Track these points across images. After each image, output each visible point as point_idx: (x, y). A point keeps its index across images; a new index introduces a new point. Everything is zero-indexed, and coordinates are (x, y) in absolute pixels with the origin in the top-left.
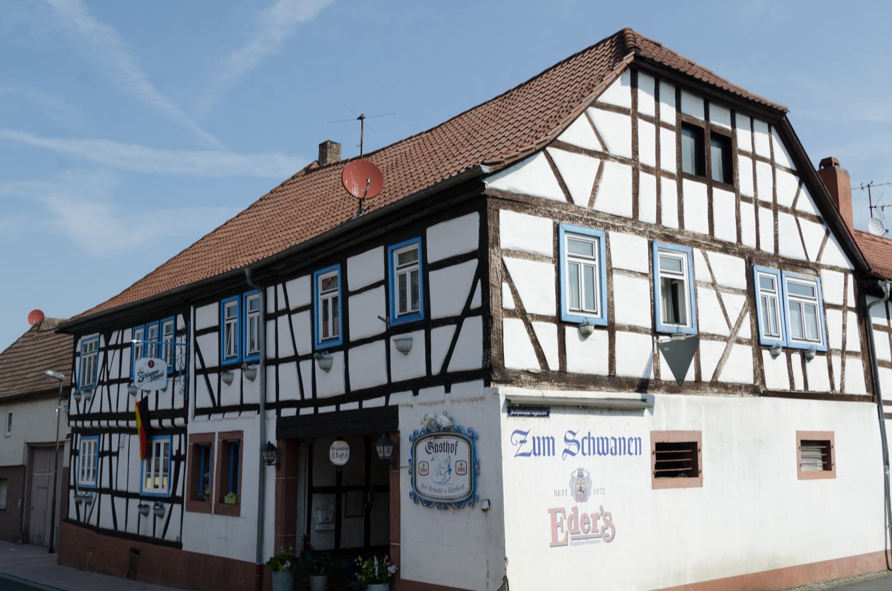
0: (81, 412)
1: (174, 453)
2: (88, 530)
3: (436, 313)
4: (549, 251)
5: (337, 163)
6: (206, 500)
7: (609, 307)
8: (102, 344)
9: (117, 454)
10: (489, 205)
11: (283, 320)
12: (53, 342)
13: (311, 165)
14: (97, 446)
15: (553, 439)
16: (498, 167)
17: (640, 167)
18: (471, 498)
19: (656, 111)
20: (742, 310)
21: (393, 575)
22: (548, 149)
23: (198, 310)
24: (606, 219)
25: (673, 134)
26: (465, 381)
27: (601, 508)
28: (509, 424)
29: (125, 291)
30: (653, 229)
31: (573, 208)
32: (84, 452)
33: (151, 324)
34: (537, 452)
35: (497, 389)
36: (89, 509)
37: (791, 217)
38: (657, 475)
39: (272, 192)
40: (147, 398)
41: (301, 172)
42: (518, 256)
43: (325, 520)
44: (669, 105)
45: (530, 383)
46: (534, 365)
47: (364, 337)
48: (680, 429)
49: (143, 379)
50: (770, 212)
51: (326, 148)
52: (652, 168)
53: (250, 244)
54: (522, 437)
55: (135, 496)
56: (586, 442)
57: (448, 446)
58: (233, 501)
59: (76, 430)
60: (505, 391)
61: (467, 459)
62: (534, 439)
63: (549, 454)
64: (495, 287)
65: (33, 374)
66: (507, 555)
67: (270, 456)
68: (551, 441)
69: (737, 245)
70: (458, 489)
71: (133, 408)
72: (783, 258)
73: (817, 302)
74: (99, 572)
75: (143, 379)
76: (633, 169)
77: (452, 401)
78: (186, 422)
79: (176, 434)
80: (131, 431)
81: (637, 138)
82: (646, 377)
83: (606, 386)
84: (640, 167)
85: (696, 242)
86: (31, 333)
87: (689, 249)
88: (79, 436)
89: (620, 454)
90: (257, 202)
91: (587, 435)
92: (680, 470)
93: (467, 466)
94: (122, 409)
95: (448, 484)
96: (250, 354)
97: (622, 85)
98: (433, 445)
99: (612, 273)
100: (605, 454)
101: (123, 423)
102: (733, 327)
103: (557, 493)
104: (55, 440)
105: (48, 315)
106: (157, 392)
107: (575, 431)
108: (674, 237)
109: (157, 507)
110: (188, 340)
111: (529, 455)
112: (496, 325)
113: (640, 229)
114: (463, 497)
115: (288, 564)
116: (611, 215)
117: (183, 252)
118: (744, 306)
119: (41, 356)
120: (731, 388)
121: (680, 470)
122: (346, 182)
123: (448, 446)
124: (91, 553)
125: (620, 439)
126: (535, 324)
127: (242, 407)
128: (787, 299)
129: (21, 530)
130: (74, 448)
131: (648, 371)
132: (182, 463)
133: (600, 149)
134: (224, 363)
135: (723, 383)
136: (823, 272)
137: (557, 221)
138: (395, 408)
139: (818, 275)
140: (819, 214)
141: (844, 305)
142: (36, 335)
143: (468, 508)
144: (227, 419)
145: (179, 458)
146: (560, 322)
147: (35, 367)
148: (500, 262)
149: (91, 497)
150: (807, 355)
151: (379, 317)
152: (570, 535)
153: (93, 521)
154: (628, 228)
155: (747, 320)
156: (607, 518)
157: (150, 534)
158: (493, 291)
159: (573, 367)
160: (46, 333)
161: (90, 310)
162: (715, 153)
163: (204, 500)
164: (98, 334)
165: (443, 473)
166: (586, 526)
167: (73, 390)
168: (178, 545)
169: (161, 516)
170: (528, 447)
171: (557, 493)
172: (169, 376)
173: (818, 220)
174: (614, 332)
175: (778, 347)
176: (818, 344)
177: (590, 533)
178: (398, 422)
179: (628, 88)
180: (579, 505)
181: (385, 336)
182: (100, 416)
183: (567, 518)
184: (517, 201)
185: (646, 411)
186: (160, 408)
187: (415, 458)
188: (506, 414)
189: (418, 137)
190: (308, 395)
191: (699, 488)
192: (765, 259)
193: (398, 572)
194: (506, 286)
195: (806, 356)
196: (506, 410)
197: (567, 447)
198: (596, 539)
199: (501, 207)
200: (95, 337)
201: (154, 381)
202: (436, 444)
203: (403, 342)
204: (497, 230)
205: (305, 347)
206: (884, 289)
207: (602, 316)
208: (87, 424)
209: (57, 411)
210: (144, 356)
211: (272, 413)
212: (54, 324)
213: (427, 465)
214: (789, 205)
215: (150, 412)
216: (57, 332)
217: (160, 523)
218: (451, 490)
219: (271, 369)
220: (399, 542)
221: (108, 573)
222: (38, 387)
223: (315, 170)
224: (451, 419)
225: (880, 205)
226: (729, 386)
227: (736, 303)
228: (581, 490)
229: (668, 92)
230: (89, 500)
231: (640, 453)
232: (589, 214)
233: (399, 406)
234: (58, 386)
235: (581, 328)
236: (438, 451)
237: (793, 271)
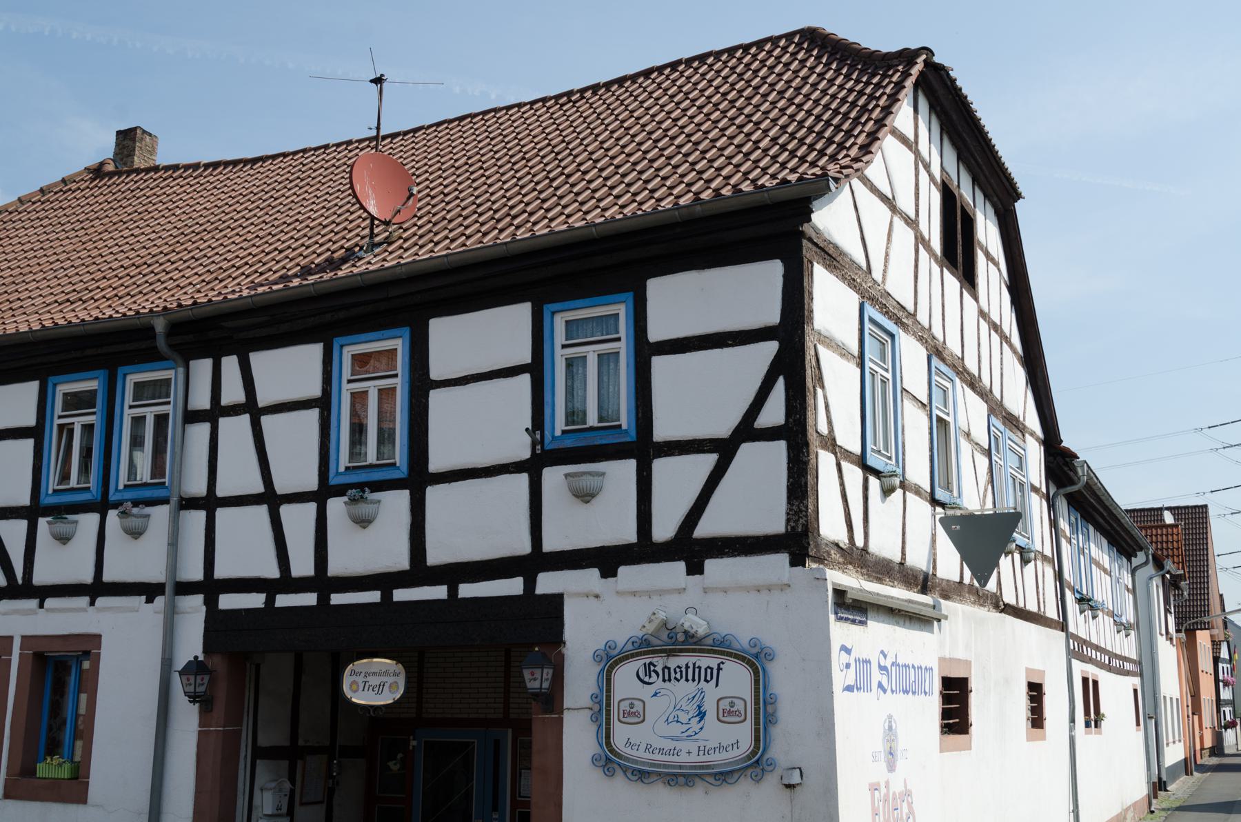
26: (739, 555)
43: (277, 810)
51: (134, 140)
57: (697, 670)
58: (65, 772)
61: (747, 693)
67: (200, 685)
70: (721, 748)
77: (706, 591)
95: (696, 740)
96: (126, 486)
98: (659, 669)
114: (736, 762)
122: (358, 188)
123: (697, 670)
138: (555, 602)
143: (744, 785)
144: (99, 610)
187: (608, 691)
191: (967, 752)
202: (666, 667)
211: (195, 603)
213: (641, 704)
233: (565, 596)
235: (883, 479)
236: (670, 680)
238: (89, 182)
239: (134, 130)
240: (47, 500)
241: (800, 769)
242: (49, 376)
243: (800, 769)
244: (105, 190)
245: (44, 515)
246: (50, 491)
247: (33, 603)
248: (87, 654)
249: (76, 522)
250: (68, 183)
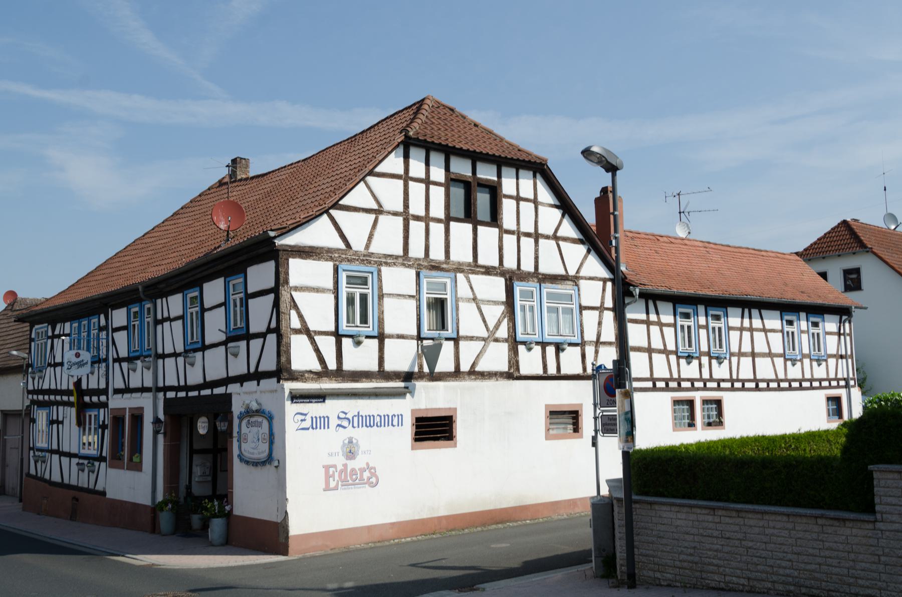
0: (36, 388)
1: (101, 423)
2: (43, 483)
3: (253, 329)
4: (330, 285)
5: (246, 179)
7: (379, 321)
8: (50, 334)
9: (62, 422)
10: (280, 256)
11: (167, 325)
13: (223, 178)
14: (48, 415)
15: (328, 418)
16: (284, 231)
17: (410, 217)
18: (269, 459)
19: (426, 174)
20: (501, 317)
21: (229, 511)
22: (331, 211)
23: (113, 312)
24: (380, 258)
25: (442, 190)
27: (368, 464)
28: (291, 409)
29: (70, 287)
30: (421, 263)
31: (351, 252)
33: (83, 320)
34: (314, 427)
35: (283, 385)
36: (44, 466)
37: (553, 243)
38: (416, 440)
39: (191, 202)
40: (81, 379)
41: (216, 184)
42: (304, 291)
44: (438, 167)
45: (312, 379)
46: (316, 366)
47: (213, 343)
48: (438, 407)
50: (531, 241)
52: (422, 217)
54: (303, 417)
55: (75, 456)
56: (356, 419)
59: (33, 402)
60: (289, 386)
61: (267, 432)
62: (312, 418)
63: (324, 428)
64: (284, 313)
66: (288, 496)
68: (326, 419)
69: (499, 268)
71: (71, 387)
72: (543, 275)
73: (574, 306)
76: (404, 219)
78: (108, 399)
80: (69, 404)
81: (408, 196)
82: (411, 371)
83: (377, 379)
84: (410, 217)
85: (460, 269)
86: (6, 312)
87: (452, 275)
88: (36, 407)
89: (385, 426)
91: (357, 414)
92: (439, 435)
93: (267, 437)
94: (64, 387)
97: (396, 157)
99: (383, 297)
100: (372, 427)
101: (65, 398)
102: (491, 330)
103: (331, 455)
104: (21, 409)
105: (21, 295)
106: (88, 375)
107: (346, 411)
108: (439, 267)
109: (89, 465)
111: (308, 429)
112: (284, 340)
113: (409, 263)
115: (170, 506)
116: (385, 255)
118: (503, 313)
119: (13, 334)
120: (487, 375)
121: (439, 435)
124: (46, 501)
125: (384, 416)
126: (317, 338)
127: (143, 390)
128: (545, 305)
131: (413, 365)
132: (106, 431)
133: (375, 207)
134: (131, 355)
135: (480, 372)
136: (582, 283)
137: (337, 263)
138: (230, 395)
139: (577, 285)
140: (581, 237)
141: (601, 306)
142: (10, 313)
143: (268, 466)
144: (134, 398)
145: (104, 427)
146: (338, 336)
147: (8, 344)
148: (289, 296)
149: (45, 457)
150: (560, 347)
151: (219, 330)
152: (340, 483)
153: (47, 476)
154: (399, 263)
155: (505, 324)
156: (373, 471)
157: (86, 486)
158: (282, 316)
159: (347, 366)
162: (482, 199)
163: (120, 459)
164: (47, 324)
165: (255, 441)
166: (354, 477)
167: (30, 370)
168: (103, 493)
169: (93, 472)
170: (307, 424)
171: (331, 455)
172: (93, 363)
173: (581, 242)
174: (384, 340)
175: (531, 343)
176: (573, 338)
177: (357, 481)
178: (231, 405)
179: (402, 159)
180: (348, 462)
181: (224, 343)
182: (49, 392)
183: (338, 471)
184: (303, 252)
185: (408, 395)
186: (90, 387)
188: (290, 402)
189: (297, 164)
190: (182, 383)
192: (524, 277)
193: (232, 510)
194: (293, 313)
195: (559, 348)
196: (290, 399)
197: (339, 422)
198: (362, 486)
199: (290, 257)
201: (80, 368)
203: (233, 349)
204: (287, 274)
205: (180, 348)
206: (634, 292)
207: (373, 329)
208: (41, 397)
211: (161, 395)
214: (551, 233)
216: (15, 321)
217: (93, 477)
218: (259, 453)
219: (160, 361)
220: (232, 489)
221: (57, 517)
224: (259, 404)
225: (687, 210)
226: (485, 374)
227: (494, 313)
228: (350, 452)
229: (437, 159)
230: (43, 459)
231: (402, 425)
232: (364, 256)
237: (552, 283)
239: (236, 159)
241: (279, 461)
243: (279, 461)
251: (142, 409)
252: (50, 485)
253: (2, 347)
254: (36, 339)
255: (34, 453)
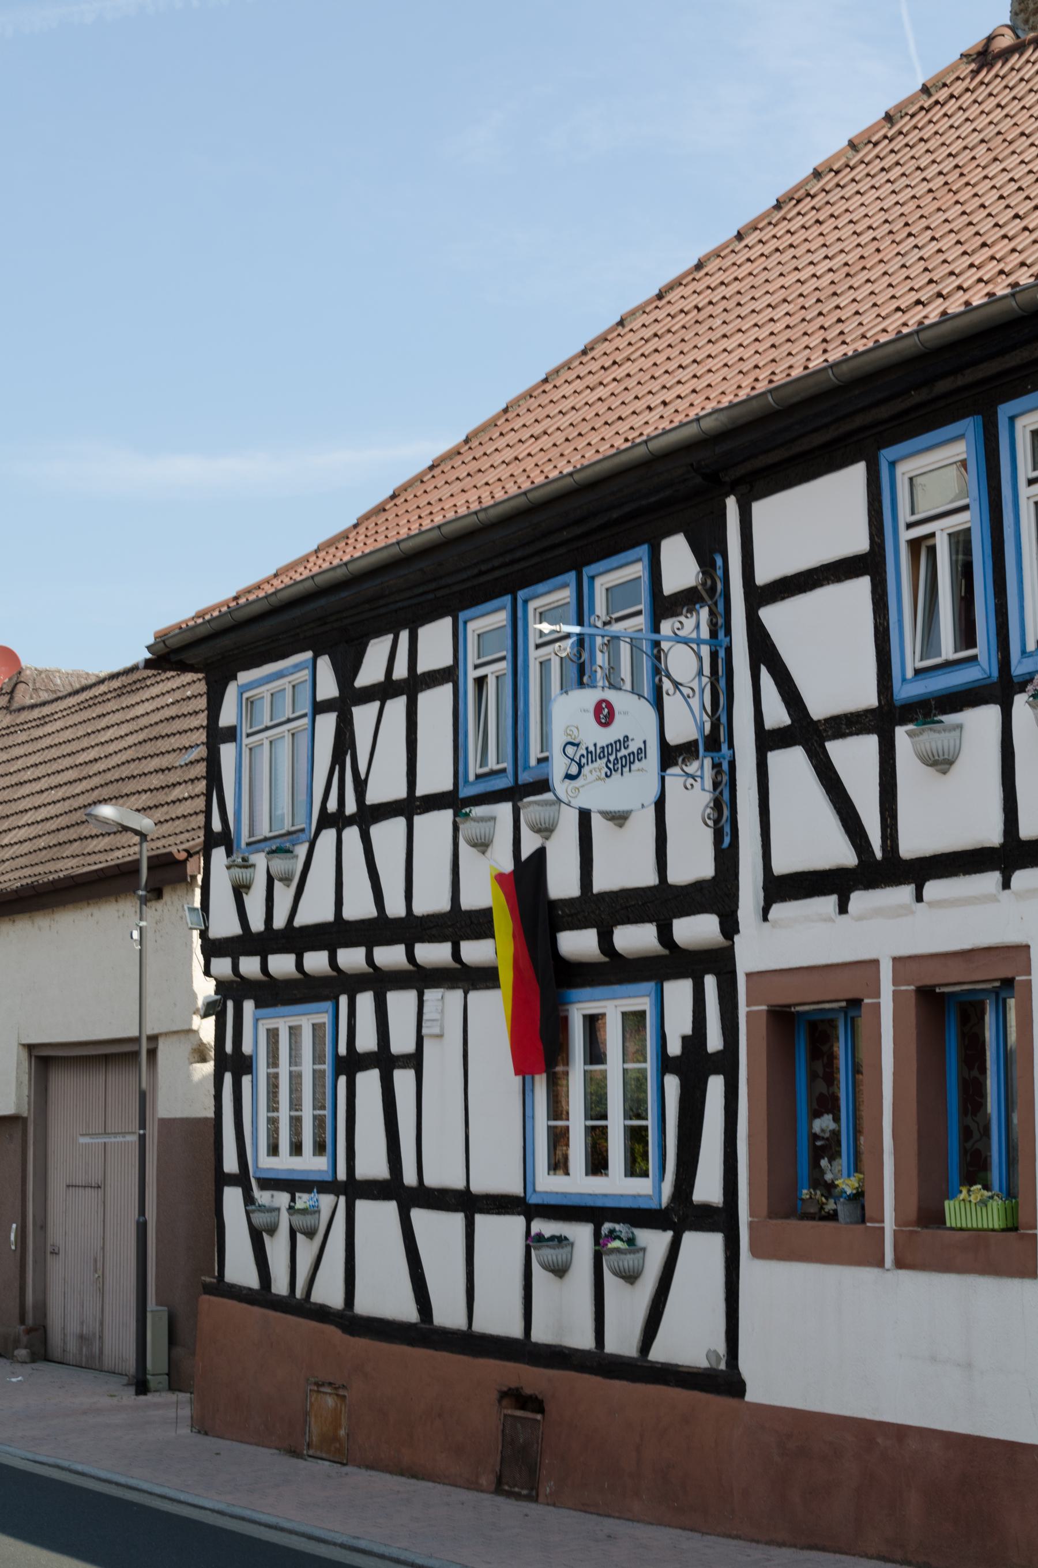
0: (257, 925)
1: (674, 1048)
6: (841, 1215)
8: (328, 688)
9: (415, 1061)
12: (68, 734)
13: (990, 39)
23: (760, 508)
32: (273, 1059)
33: (540, 588)
36: (306, 1251)
40: (540, 855)
49: (580, 767)
53: (429, 509)
58: (993, 1216)
65: (22, 834)
74: (370, 1466)
75: (580, 767)
78: (730, 927)
79: (678, 975)
88: (249, 1006)
90: (806, 182)
110: (721, 626)
117: (557, 371)
124: (330, 1401)
129: (22, 1320)
130: (229, 1048)
132: (716, 1085)
149: (315, 1211)
157: (585, 1341)
160: (36, 713)
161: (258, 587)
164: (309, 655)
200: (298, 668)
201: (616, 776)
208: (282, 964)
209: (136, 935)
210: (581, 684)
212: (52, 687)
215: (554, 905)
222: (51, 867)
223: (1006, 54)
234: (137, 857)
238: (968, 80)
240: (904, 692)
242: (879, 448)
244: (997, 86)
245: (903, 722)
246: (910, 674)
247: (906, 892)
248: (1008, 983)
249: (960, 727)
250: (932, 90)
251: (624, 1015)
252: (352, 1334)
253: (6, 825)
254: (245, 729)
255: (249, 1199)
